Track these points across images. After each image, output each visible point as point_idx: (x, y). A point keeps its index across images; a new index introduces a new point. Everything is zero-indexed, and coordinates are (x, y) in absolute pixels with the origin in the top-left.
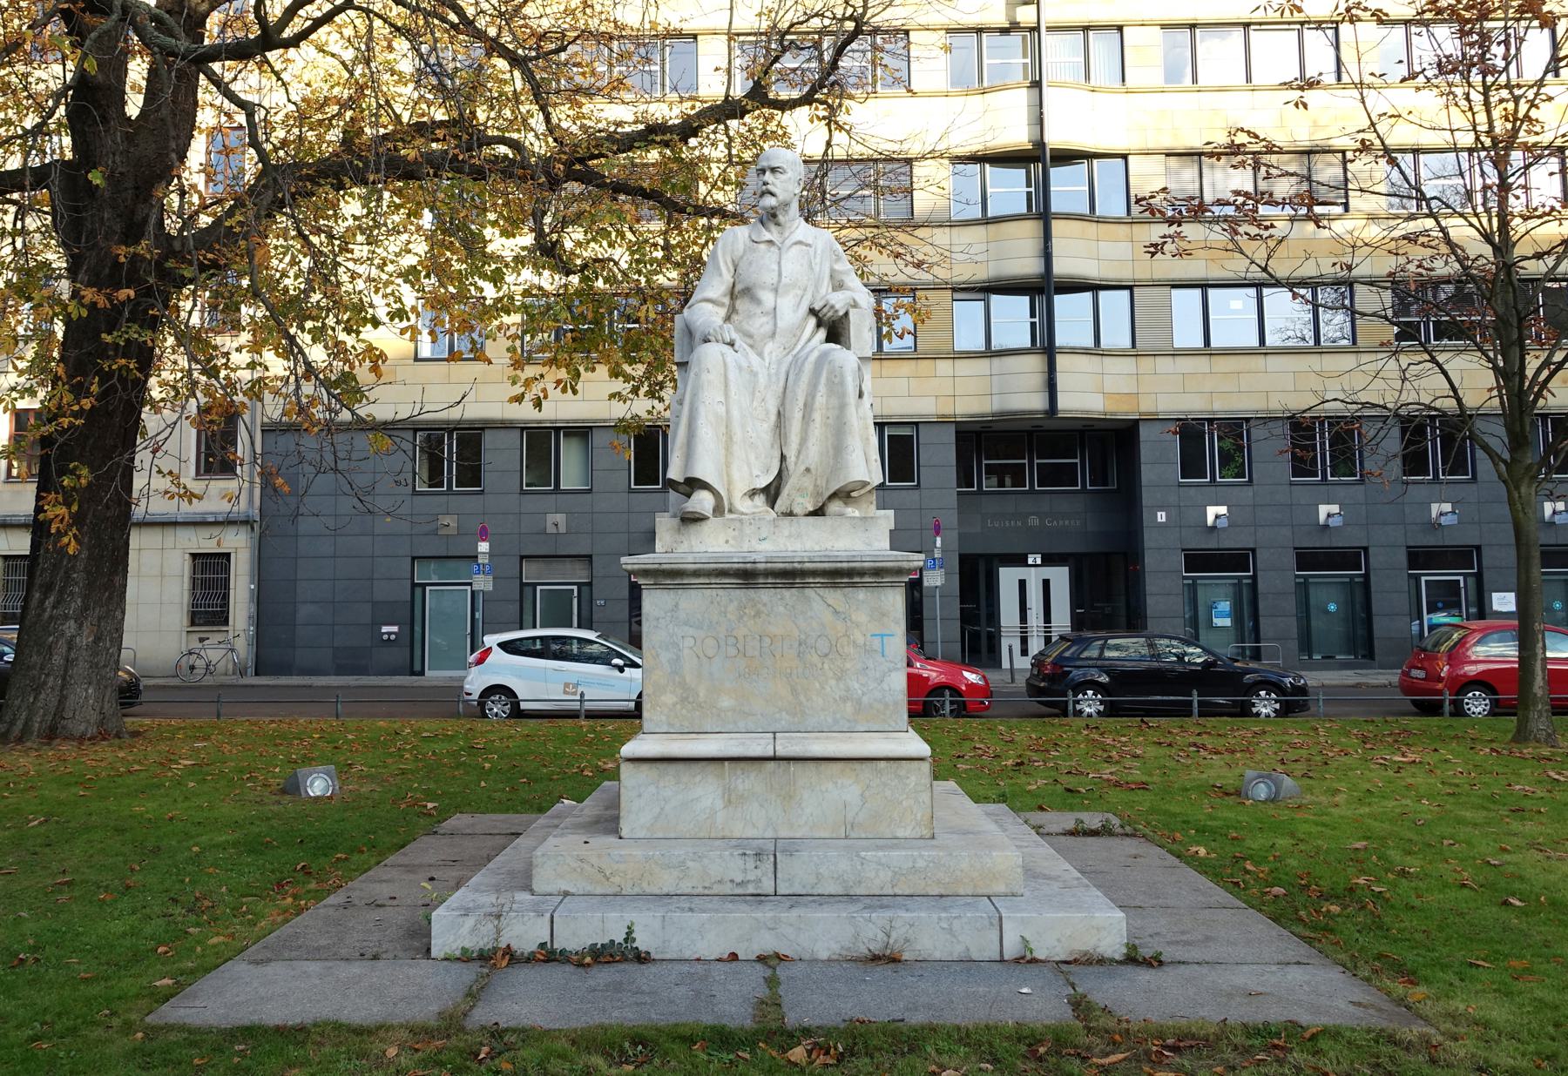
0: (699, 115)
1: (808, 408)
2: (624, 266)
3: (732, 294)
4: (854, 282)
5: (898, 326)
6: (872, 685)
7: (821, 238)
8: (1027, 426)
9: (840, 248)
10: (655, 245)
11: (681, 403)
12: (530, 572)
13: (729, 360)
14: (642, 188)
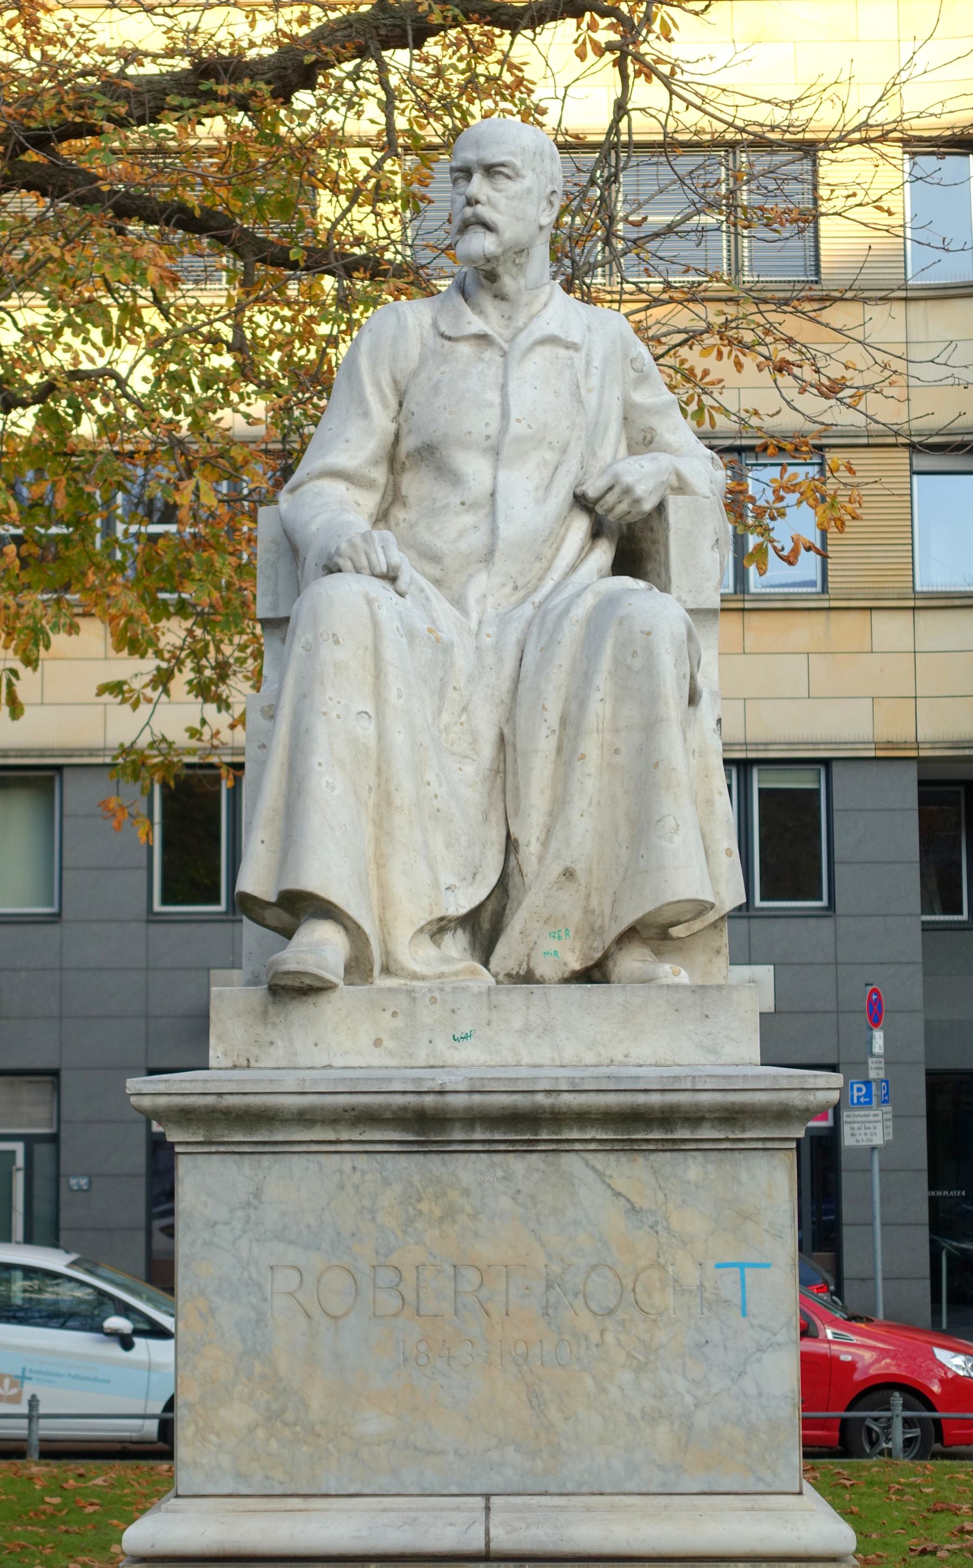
0: (320, 37)
1: (570, 726)
2: (139, 387)
3: (394, 460)
4: (679, 432)
5: (782, 533)
7: (598, 331)
9: (642, 351)
10: (214, 340)
11: (271, 713)
14: (182, 209)
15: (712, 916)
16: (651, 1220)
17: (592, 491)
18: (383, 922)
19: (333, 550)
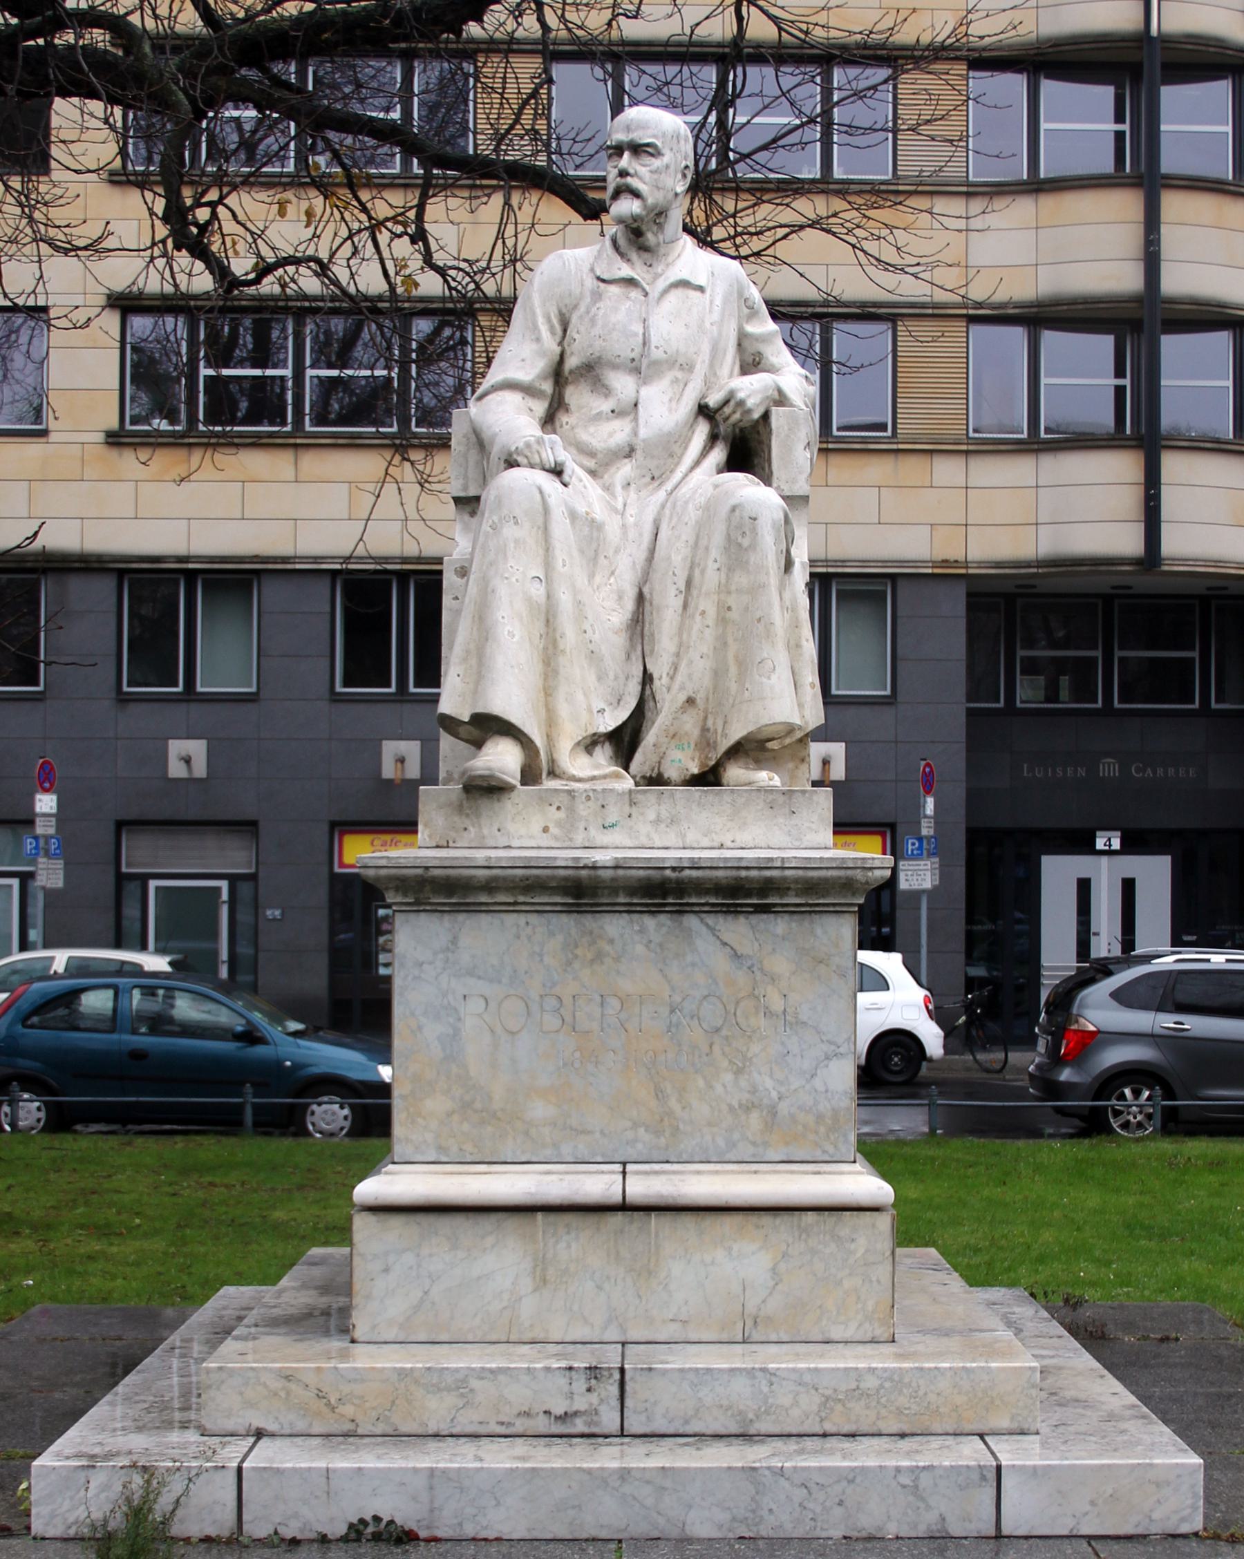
3: (559, 375)
6: (796, 1083)
8: (1102, 585)
12: (139, 854)
13: (552, 501)
15: (799, 734)
16: (750, 963)
17: (713, 400)
18: (549, 738)
19: (513, 449)
